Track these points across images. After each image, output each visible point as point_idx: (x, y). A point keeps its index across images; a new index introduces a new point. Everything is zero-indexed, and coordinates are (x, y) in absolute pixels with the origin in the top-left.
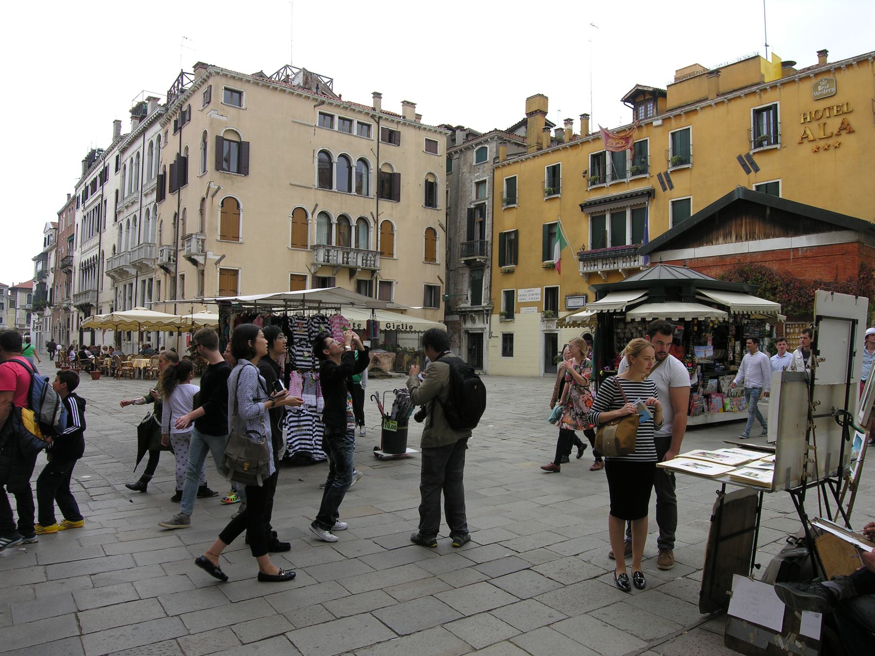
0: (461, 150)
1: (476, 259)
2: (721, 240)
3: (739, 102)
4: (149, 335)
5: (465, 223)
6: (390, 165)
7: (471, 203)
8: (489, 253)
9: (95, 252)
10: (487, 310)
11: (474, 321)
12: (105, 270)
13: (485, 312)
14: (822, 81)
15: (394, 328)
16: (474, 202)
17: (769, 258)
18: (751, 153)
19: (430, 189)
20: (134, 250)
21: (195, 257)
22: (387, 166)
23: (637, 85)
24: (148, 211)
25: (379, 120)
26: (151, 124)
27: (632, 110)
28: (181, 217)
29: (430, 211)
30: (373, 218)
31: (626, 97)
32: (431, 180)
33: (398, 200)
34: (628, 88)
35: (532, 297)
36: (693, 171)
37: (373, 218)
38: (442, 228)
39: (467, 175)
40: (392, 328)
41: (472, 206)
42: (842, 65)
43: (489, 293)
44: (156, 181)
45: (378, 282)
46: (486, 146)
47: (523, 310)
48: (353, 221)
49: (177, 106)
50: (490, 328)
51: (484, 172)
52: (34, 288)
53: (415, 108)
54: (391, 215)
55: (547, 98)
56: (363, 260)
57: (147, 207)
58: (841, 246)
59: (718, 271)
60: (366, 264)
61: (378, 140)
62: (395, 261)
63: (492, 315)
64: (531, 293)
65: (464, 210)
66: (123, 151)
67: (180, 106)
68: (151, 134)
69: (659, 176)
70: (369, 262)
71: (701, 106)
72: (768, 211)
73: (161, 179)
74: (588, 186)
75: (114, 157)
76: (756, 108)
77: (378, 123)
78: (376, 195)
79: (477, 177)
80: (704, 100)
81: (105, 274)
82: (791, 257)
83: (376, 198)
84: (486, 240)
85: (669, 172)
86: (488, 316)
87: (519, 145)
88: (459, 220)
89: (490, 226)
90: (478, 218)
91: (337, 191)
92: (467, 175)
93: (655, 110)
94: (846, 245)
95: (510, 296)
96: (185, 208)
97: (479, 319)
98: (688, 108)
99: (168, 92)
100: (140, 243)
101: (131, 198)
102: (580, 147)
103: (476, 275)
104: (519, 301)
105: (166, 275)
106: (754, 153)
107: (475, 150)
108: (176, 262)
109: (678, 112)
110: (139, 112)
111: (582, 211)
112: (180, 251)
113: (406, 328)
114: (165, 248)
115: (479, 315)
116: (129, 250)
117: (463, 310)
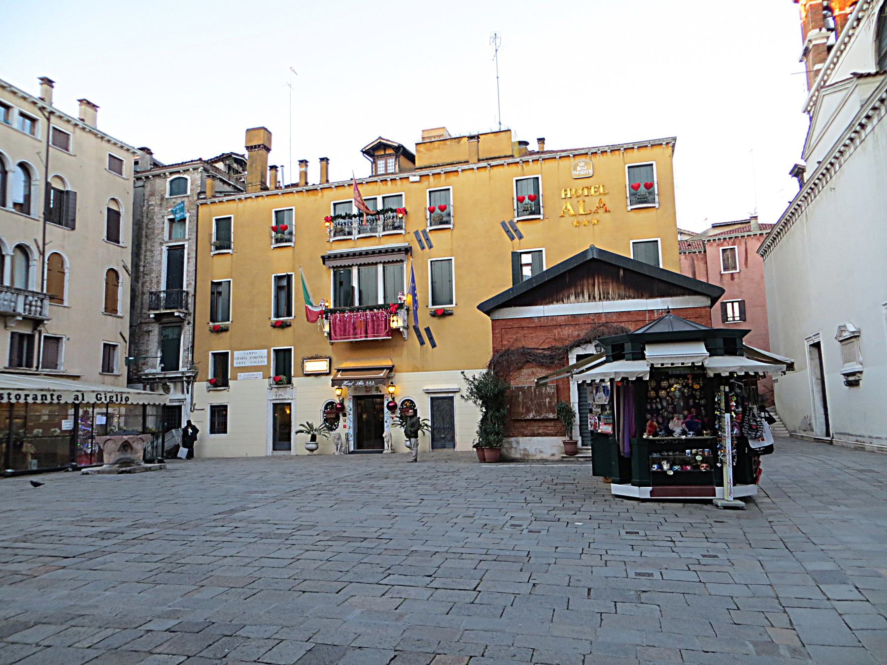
0: (147, 178)
1: (173, 313)
2: (572, 298)
3: (501, 169)
10: (188, 377)
11: (167, 390)
13: (185, 379)
14: (580, 162)
15: (106, 400)
17: (624, 318)
18: (515, 220)
19: (113, 217)
22: (58, 180)
23: (380, 138)
25: (49, 116)
27: (371, 163)
29: (112, 246)
30: (38, 247)
31: (367, 148)
32: (114, 207)
34: (369, 140)
35: (255, 360)
36: (454, 231)
37: (38, 247)
38: (127, 271)
40: (103, 400)
42: (664, 141)
43: (190, 355)
45: (42, 338)
46: (185, 176)
47: (241, 375)
50: (192, 398)
56: (25, 304)
58: (695, 310)
59: (570, 331)
60: (30, 310)
61: (48, 142)
62: (66, 309)
63: (195, 383)
64: (254, 355)
69: (416, 233)
70: (33, 308)
71: (463, 168)
72: (621, 272)
77: (48, 119)
78: (42, 216)
80: (456, 163)
82: (647, 319)
83: (42, 220)
85: (428, 231)
86: (188, 385)
92: (157, 209)
93: (397, 166)
94: (699, 310)
95: (221, 360)
97: (175, 388)
98: (449, 169)
102: (320, 194)
103: (171, 334)
104: (235, 365)
106: (518, 221)
107: (169, 180)
109: (438, 170)
111: (324, 263)
113: (121, 400)
115: (175, 383)
117: (150, 377)
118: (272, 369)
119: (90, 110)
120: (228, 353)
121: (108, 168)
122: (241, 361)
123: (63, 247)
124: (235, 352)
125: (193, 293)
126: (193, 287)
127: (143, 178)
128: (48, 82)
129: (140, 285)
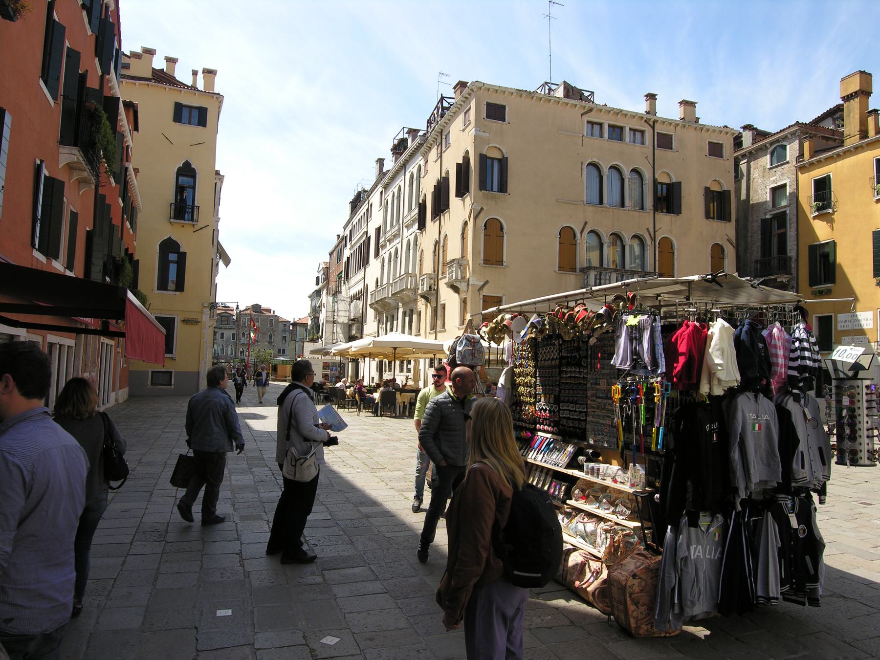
4: (409, 366)
5: (758, 236)
6: (668, 175)
7: (766, 214)
8: (794, 271)
9: (360, 286)
12: (369, 303)
16: (770, 211)
20: (395, 281)
21: (457, 284)
24: (409, 241)
26: (412, 155)
28: (441, 244)
30: (650, 234)
33: (679, 212)
37: (650, 234)
38: (731, 244)
39: (760, 181)
41: (768, 217)
44: (417, 211)
46: (784, 143)
48: (627, 239)
49: (438, 132)
51: (782, 174)
52: (309, 323)
53: (695, 107)
54: (671, 231)
55: (870, 75)
57: (408, 238)
65: (757, 221)
66: (386, 187)
67: (440, 131)
68: (412, 169)
73: (422, 207)
74: (874, 196)
75: (378, 193)
76: (816, 178)
78: (652, 208)
79: (774, 181)
81: (368, 306)
83: (652, 212)
84: (789, 255)
87: (827, 139)
88: (749, 234)
89: (794, 238)
90: (776, 231)
91: (608, 206)
96: (446, 235)
99: (428, 121)
100: (402, 274)
101: (394, 230)
104: (839, 328)
105: (426, 305)
108: (437, 291)
110: (399, 148)
112: (441, 279)
114: (425, 276)
116: (391, 282)
118: (38, 235)
119: (689, 108)
120: (831, 316)
121: (708, 155)
122: (845, 324)
123: (671, 231)
124: (838, 315)
125: (795, 257)
126: (796, 252)
127: (747, 154)
128: (651, 97)
129: (748, 255)
